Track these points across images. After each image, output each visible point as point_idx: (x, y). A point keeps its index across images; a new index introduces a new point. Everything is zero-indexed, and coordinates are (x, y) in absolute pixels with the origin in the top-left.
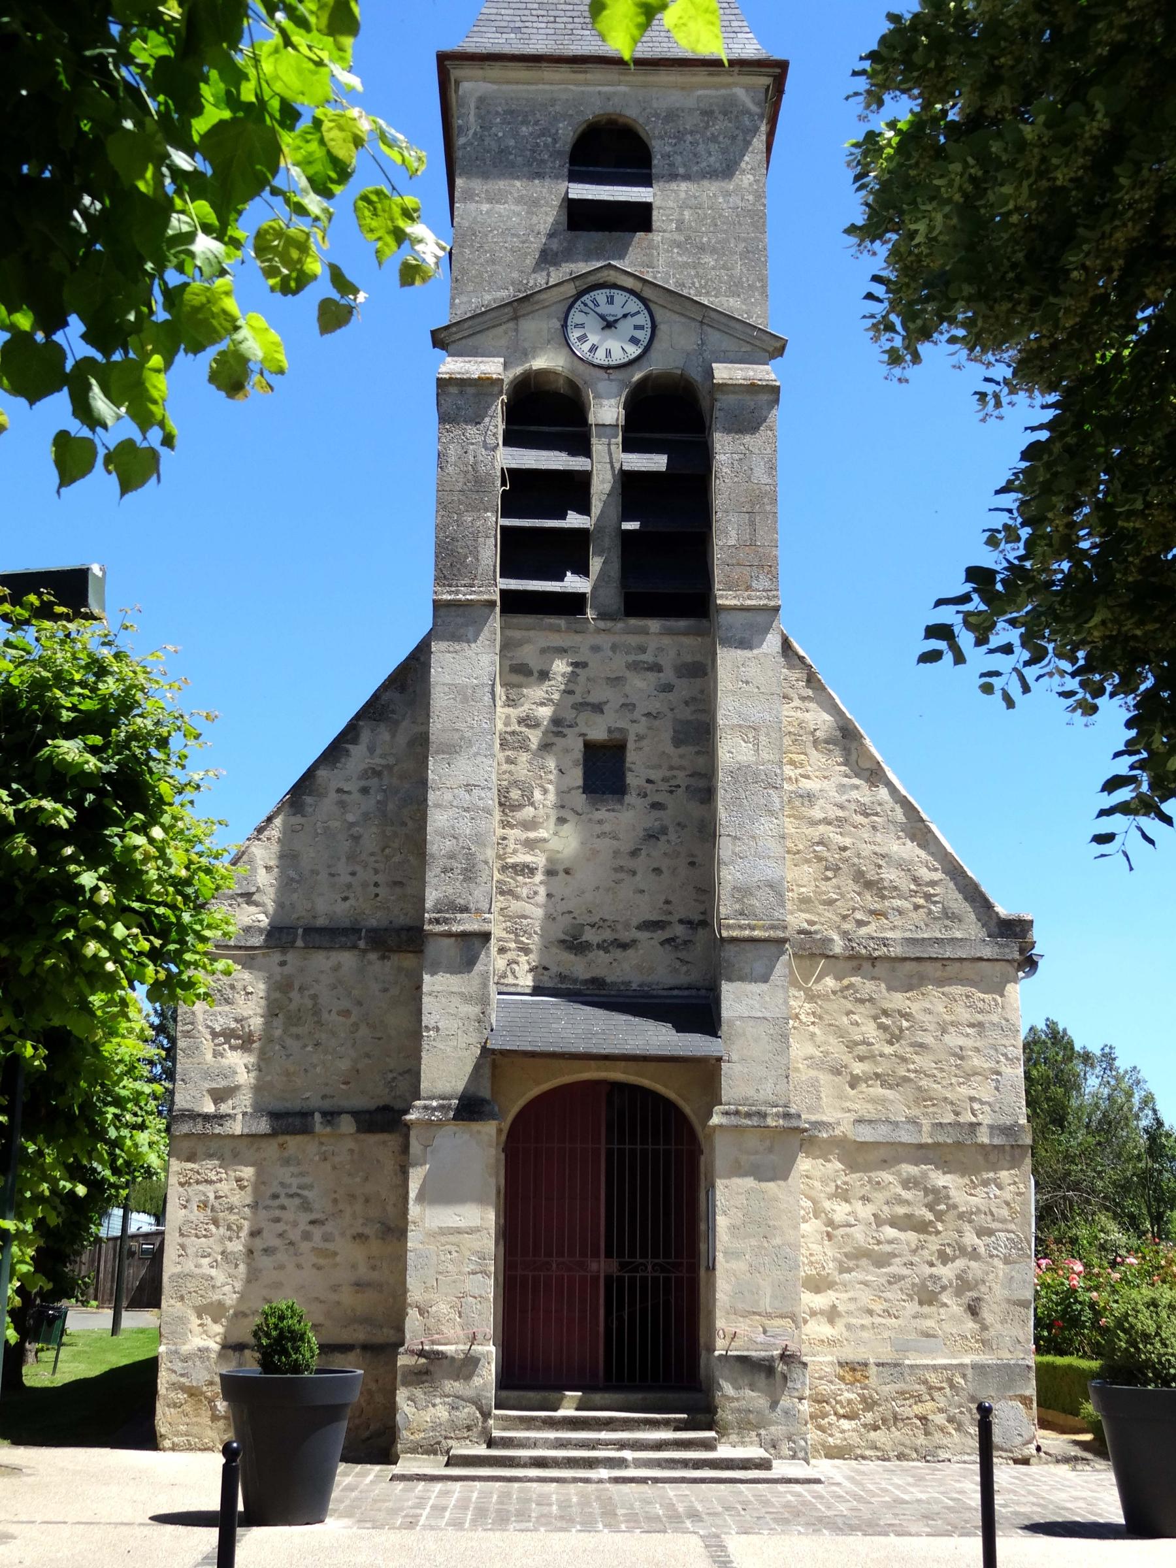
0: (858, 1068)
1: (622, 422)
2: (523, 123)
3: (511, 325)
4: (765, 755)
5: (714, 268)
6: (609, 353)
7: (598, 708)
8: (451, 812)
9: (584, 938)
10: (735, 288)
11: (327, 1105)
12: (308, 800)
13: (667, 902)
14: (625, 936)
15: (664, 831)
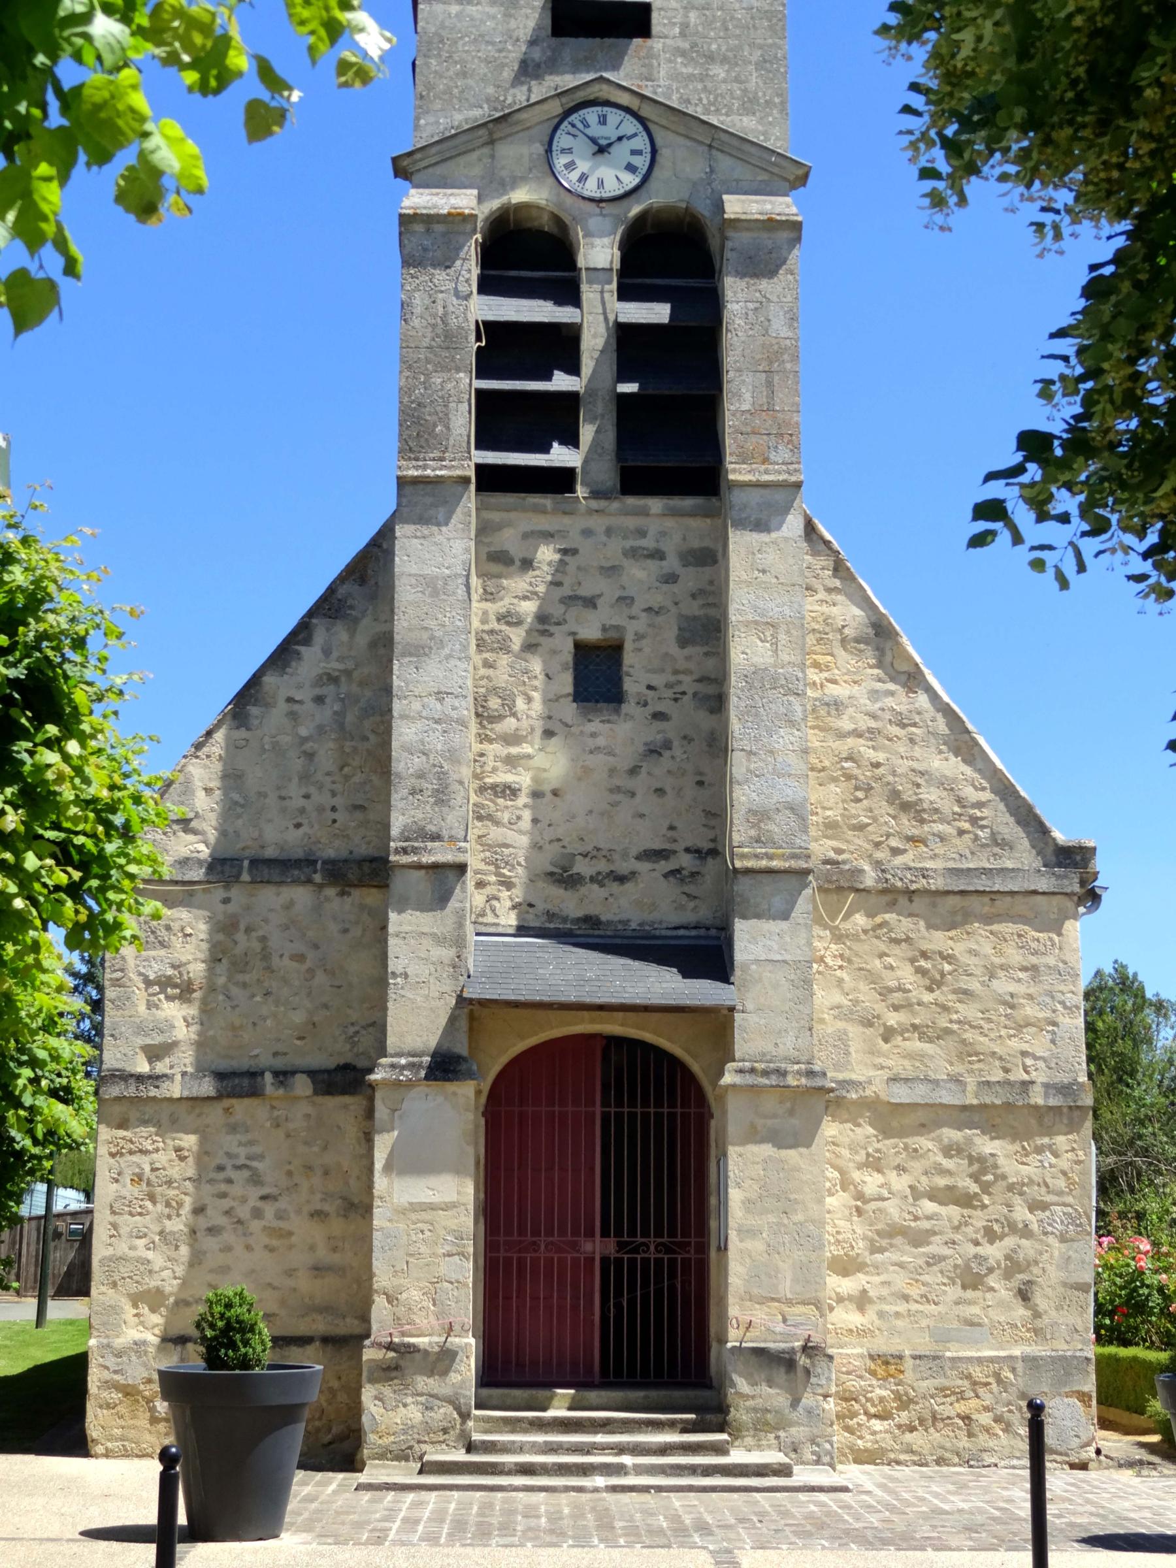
5: (724, 81)
7: (590, 603)
9: (575, 870)
11: (279, 1063)
12: (254, 710)
13: (672, 828)
14: (623, 867)
15: (667, 745)
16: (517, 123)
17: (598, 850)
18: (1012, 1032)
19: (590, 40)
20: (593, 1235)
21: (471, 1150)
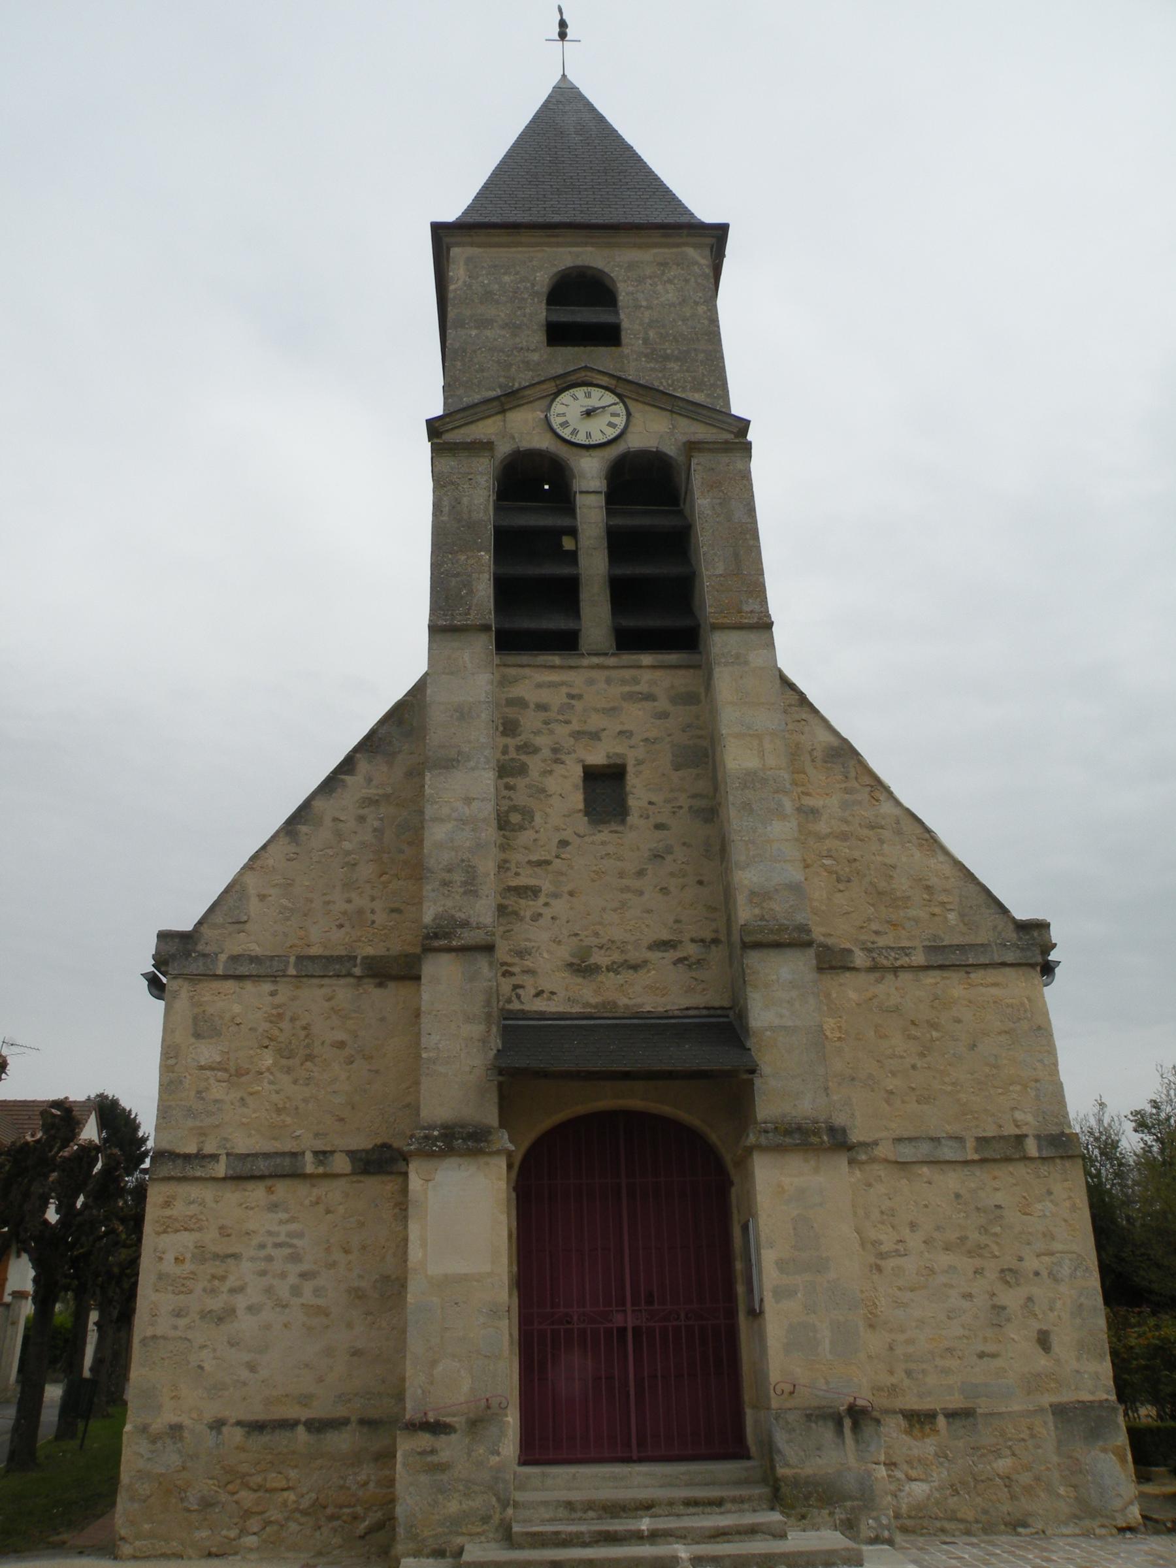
0: (891, 1083)
1: (604, 489)
2: (505, 274)
3: (499, 417)
4: (771, 761)
5: (678, 372)
6: (589, 435)
7: (595, 736)
8: (449, 826)
9: (592, 961)
10: (698, 387)
11: (320, 1145)
12: (303, 829)
13: (677, 921)
14: (634, 956)
15: (669, 850)
16: (523, 397)
17: (613, 942)
18: (1000, 1091)
19: (576, 349)
20: (624, 1304)
21: (503, 1218)
